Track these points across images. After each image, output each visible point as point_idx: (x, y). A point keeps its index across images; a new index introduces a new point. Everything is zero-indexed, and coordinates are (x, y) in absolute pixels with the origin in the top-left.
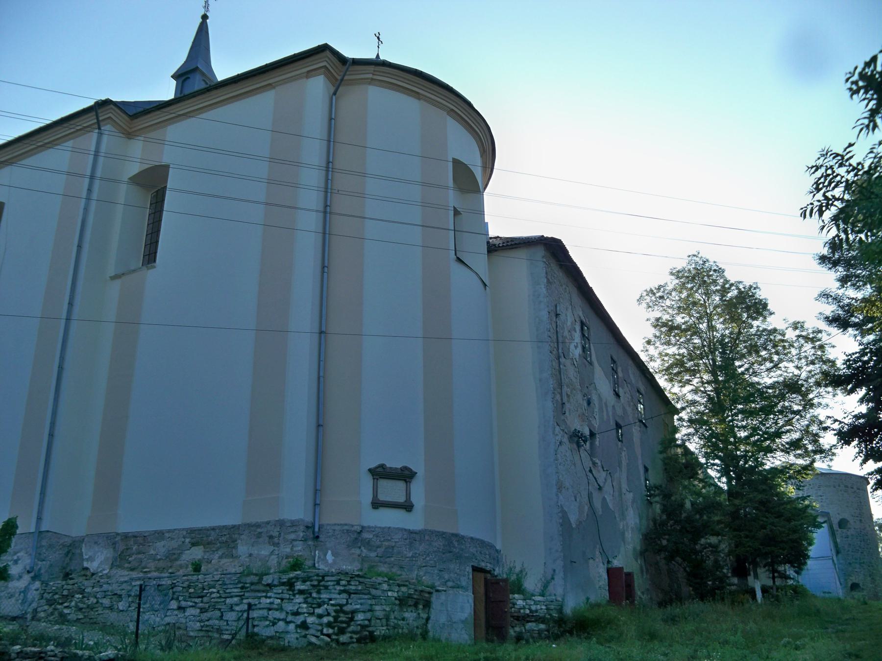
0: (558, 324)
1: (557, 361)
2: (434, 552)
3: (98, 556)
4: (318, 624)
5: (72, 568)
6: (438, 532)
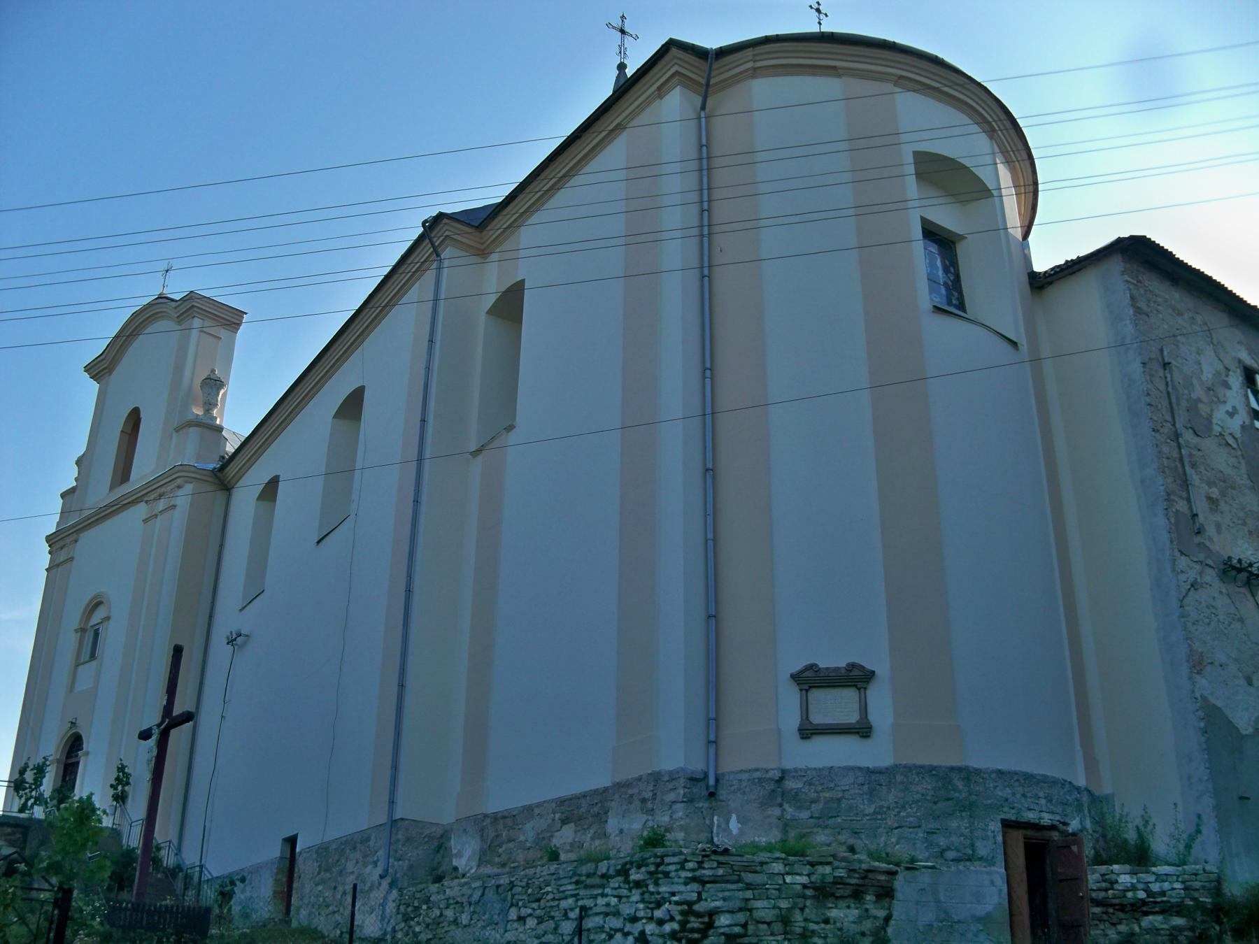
0: (1169, 379)
1: (1174, 444)
2: (916, 802)
3: (466, 849)
4: (658, 935)
5: (444, 869)
6: (922, 767)
